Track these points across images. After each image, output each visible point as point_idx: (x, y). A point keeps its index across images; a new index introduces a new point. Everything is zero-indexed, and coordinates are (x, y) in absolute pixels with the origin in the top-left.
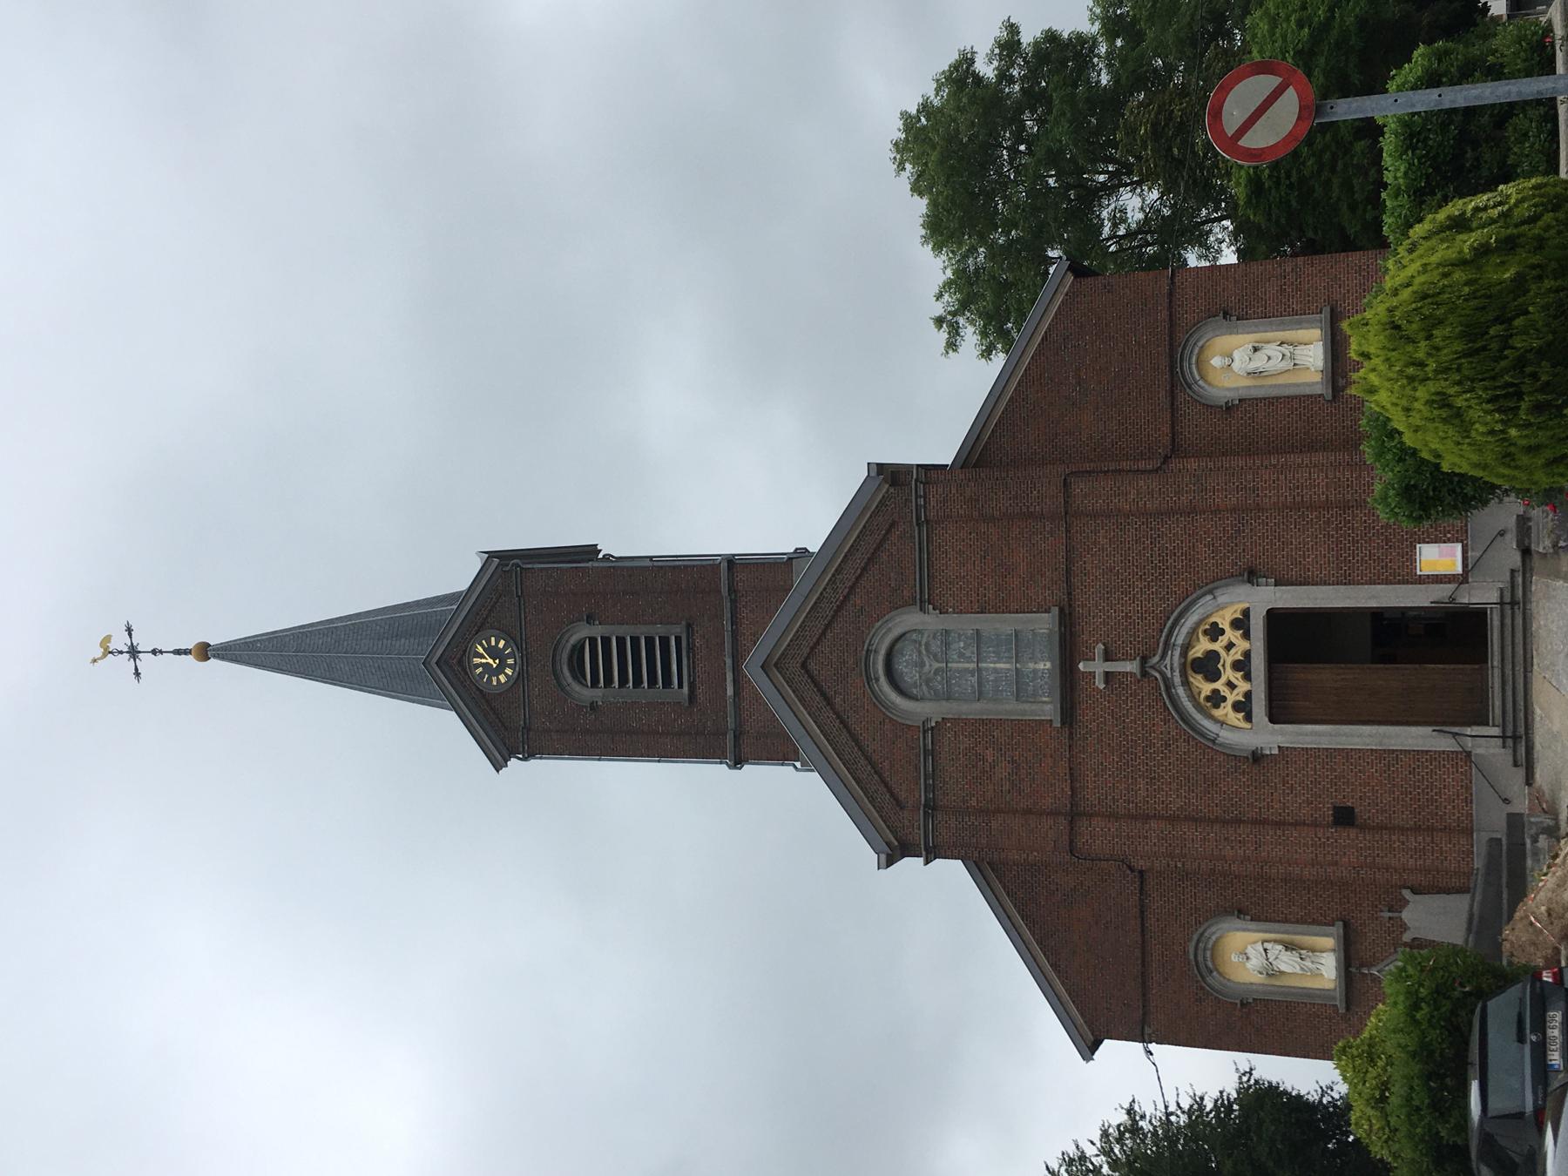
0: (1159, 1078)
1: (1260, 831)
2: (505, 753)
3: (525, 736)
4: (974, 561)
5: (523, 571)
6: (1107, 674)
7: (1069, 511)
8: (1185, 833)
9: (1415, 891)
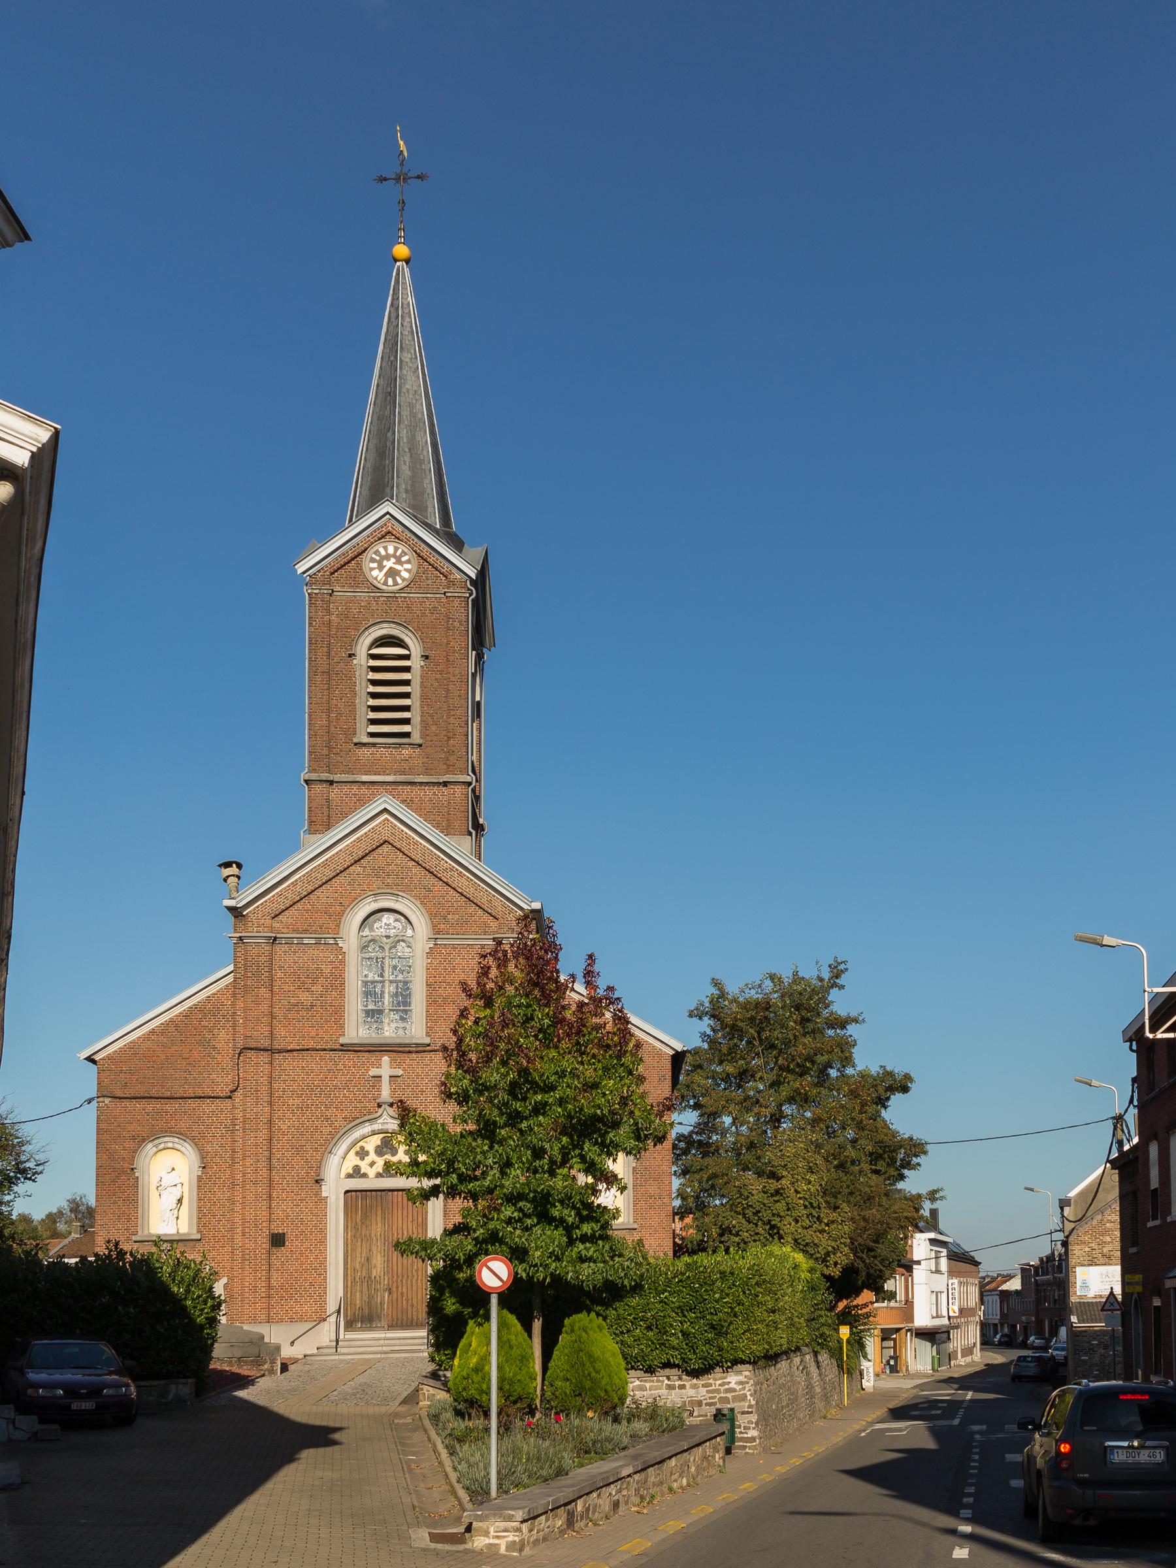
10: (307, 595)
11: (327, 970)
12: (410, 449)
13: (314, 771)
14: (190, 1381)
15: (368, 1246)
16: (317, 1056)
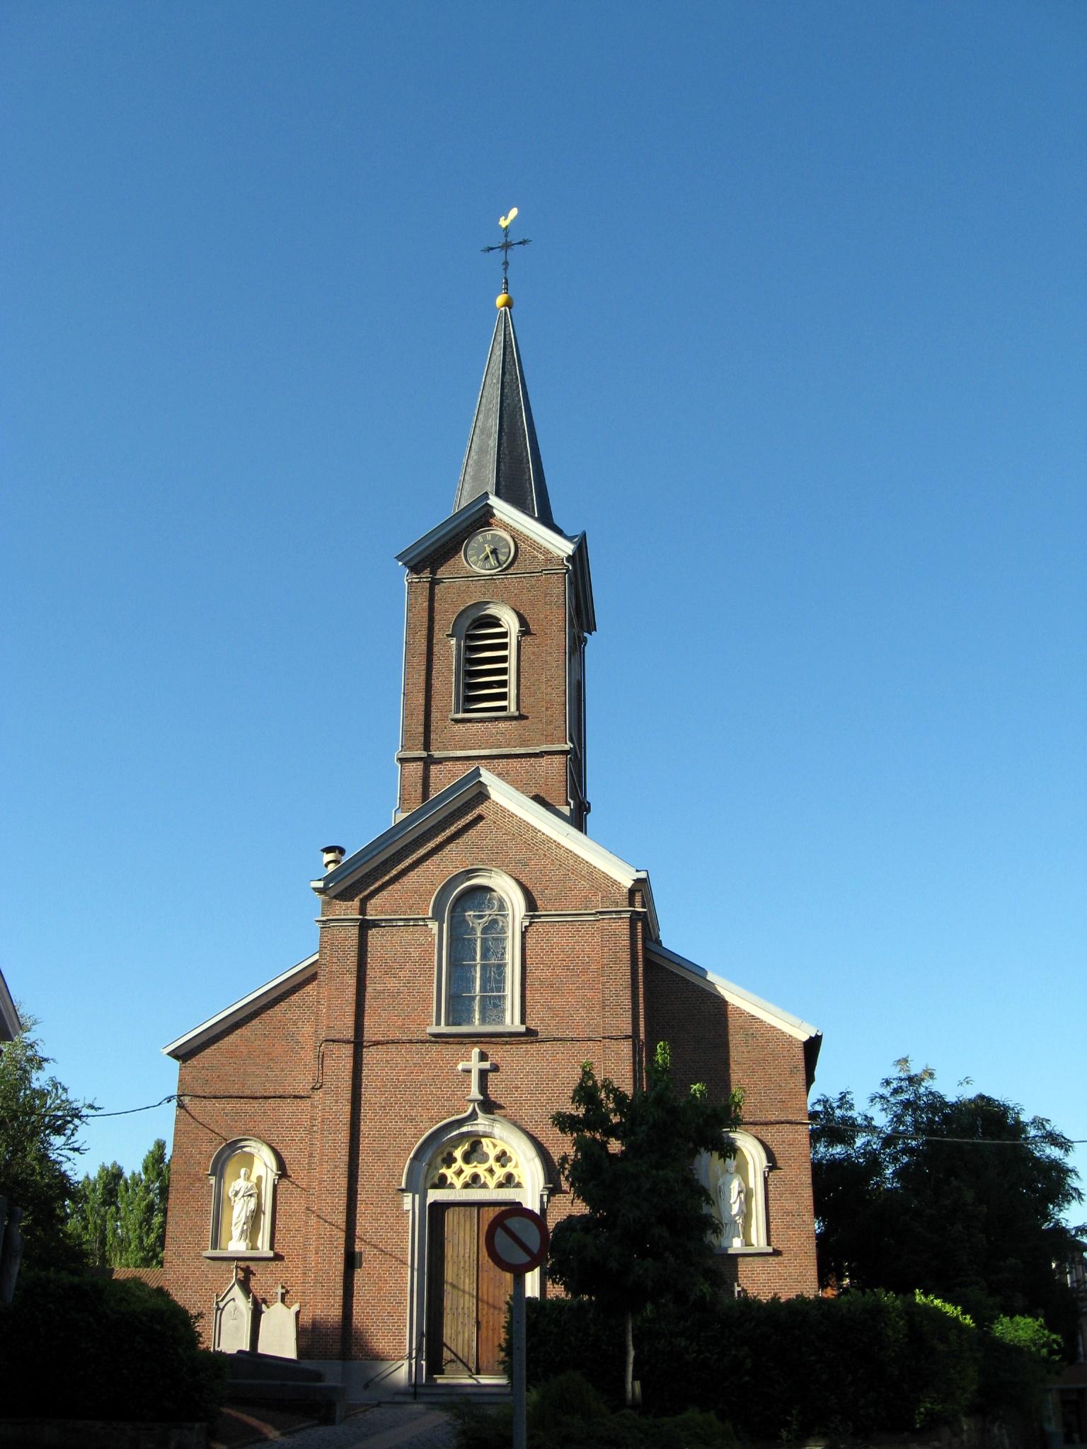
0: (148, 1108)
1: (342, 1193)
2: (412, 564)
3: (425, 580)
4: (565, 961)
5: (563, 575)
6: (469, 1071)
7: (605, 1040)
8: (340, 1133)
9: (298, 1314)
10: (406, 583)
11: (415, 954)
12: (509, 452)
13: (410, 749)
14: (197, 1426)
15: (455, 1269)
16: (403, 1049)
